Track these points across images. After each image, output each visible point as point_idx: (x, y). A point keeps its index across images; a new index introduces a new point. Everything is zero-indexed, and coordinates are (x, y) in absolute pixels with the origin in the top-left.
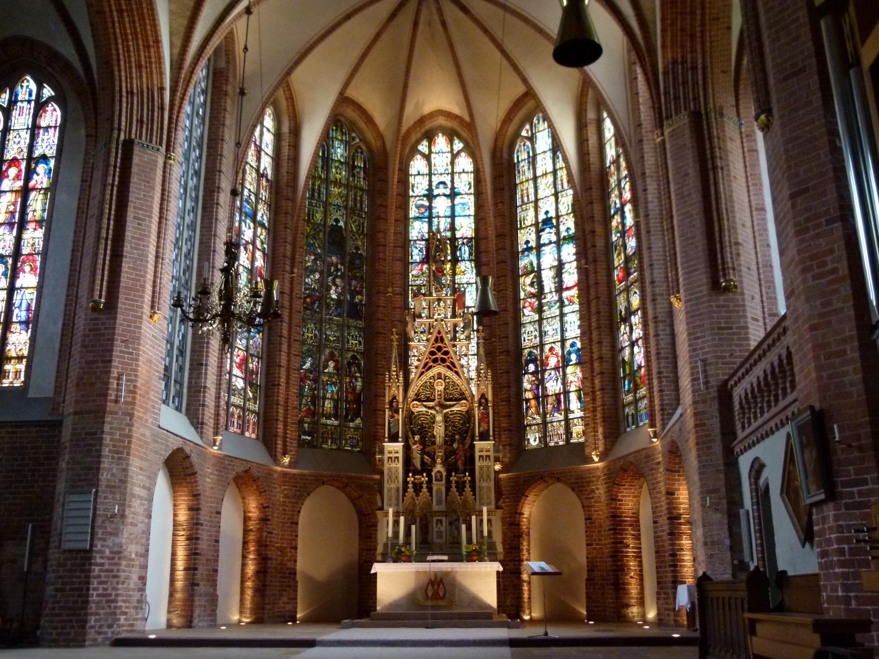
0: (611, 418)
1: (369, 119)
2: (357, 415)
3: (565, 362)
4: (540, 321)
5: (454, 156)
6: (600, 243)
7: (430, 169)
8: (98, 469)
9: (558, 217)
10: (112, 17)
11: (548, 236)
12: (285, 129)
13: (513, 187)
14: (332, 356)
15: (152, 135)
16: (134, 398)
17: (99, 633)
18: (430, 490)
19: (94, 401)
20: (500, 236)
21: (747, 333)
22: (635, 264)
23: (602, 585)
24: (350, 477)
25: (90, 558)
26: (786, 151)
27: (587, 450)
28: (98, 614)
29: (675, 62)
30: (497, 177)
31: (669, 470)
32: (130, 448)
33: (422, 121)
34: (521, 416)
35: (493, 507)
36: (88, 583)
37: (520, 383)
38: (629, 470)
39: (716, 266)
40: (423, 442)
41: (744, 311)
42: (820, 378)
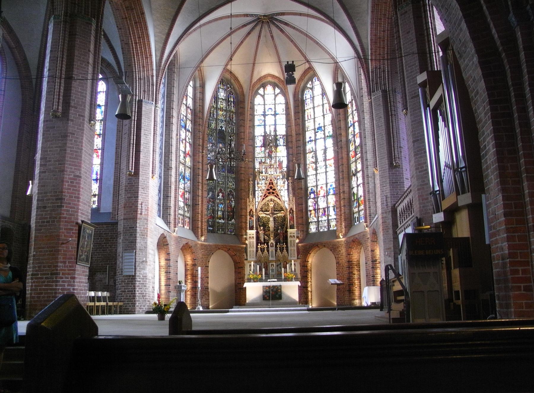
0: (349, 220)
1: (236, 79)
2: (233, 218)
3: (327, 194)
4: (316, 174)
5: (276, 96)
6: (344, 139)
7: (264, 102)
8: (136, 242)
9: (324, 126)
10: (133, 46)
11: (320, 135)
12: (198, 85)
13: (304, 111)
14: (221, 190)
15: (149, 97)
16: (148, 213)
17: (140, 309)
18: (268, 251)
19: (132, 214)
20: (298, 134)
21: (403, 185)
22: (359, 150)
23: (344, 291)
24: (231, 246)
25: (135, 279)
26: (412, 125)
27: (337, 233)
28: (139, 301)
29: (376, 68)
30: (296, 106)
31: (372, 241)
32: (147, 233)
33: (260, 79)
34: (307, 218)
35: (296, 258)
36: (135, 288)
37: (307, 203)
38: (356, 242)
39: (392, 157)
40: (264, 230)
41: (403, 175)
42: (420, 207)
